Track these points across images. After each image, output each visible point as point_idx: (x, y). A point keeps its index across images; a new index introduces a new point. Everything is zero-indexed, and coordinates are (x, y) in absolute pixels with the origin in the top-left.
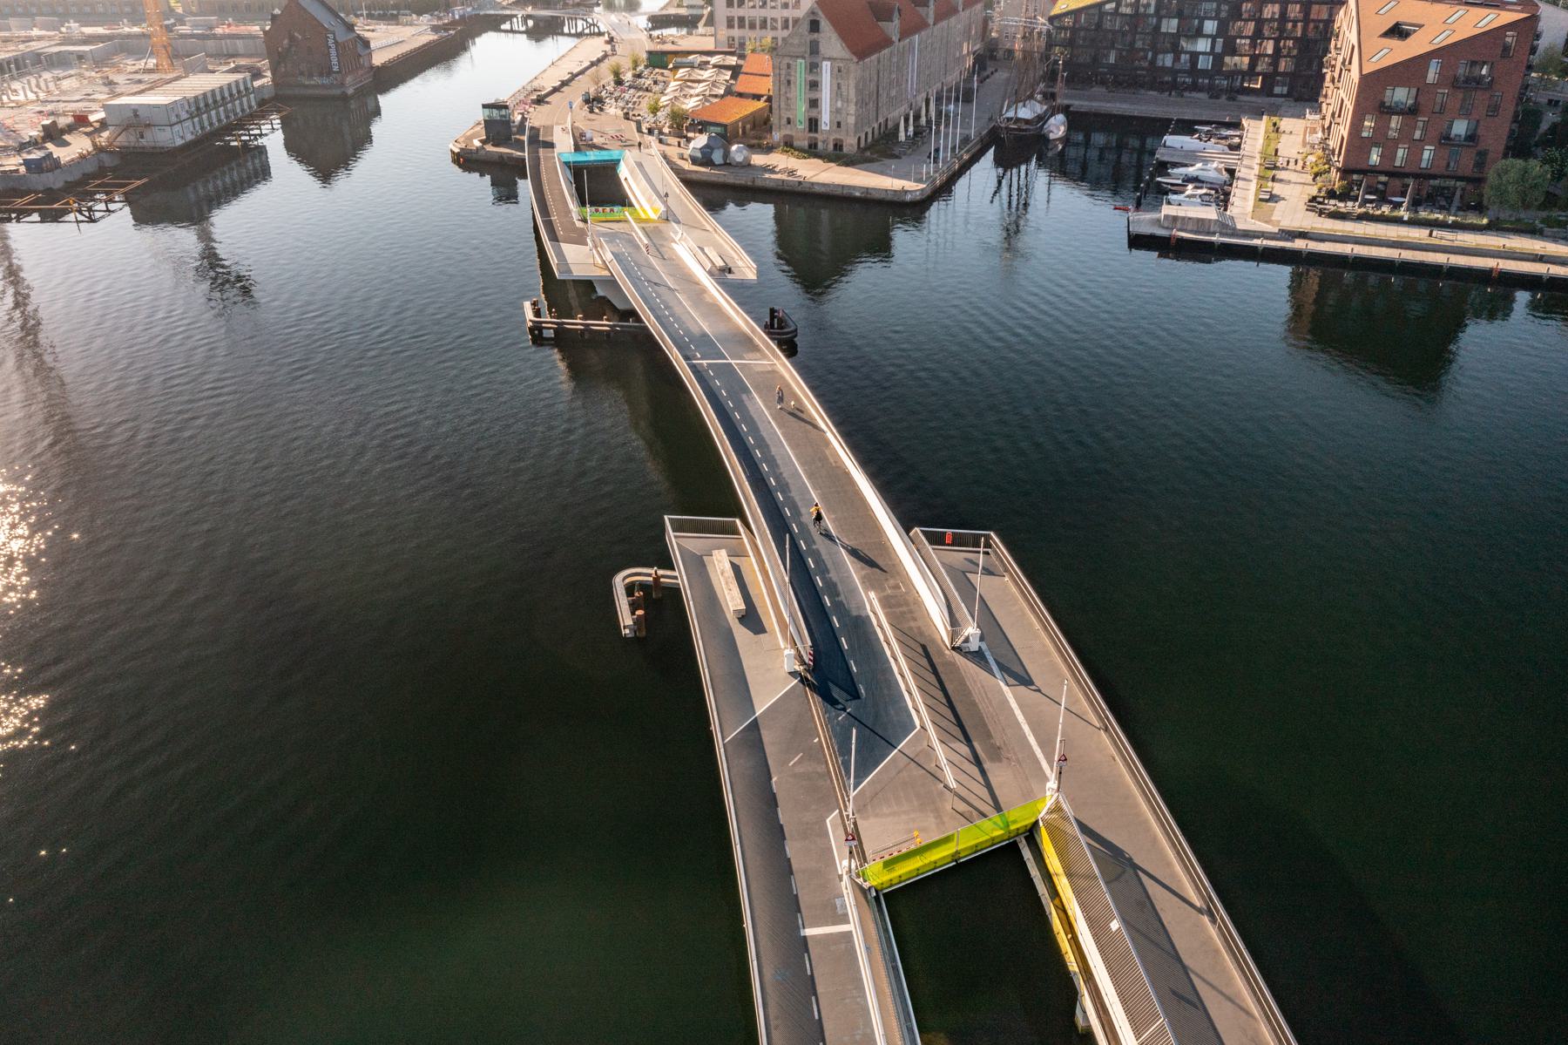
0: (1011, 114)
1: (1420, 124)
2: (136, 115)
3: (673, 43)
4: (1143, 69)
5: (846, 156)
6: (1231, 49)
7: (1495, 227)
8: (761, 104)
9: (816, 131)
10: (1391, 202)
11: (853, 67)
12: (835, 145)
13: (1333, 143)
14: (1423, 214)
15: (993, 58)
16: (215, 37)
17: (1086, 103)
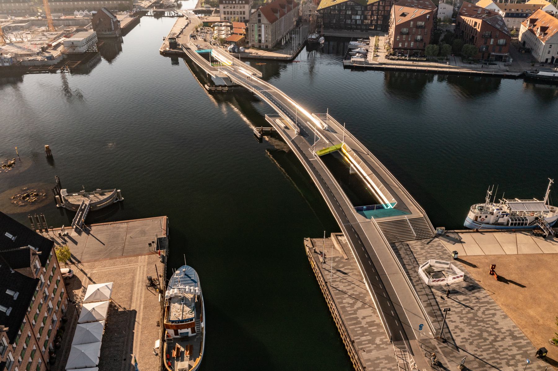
0: (310, 37)
1: (410, 37)
2: (73, 43)
3: (206, 19)
4: (343, 24)
5: (269, 49)
6: (365, 18)
7: (427, 61)
8: (243, 36)
9: (261, 43)
10: (404, 56)
11: (270, 26)
12: (266, 47)
13: (391, 42)
14: (412, 58)
15: (301, 21)
16: (62, 20)
17: (328, 34)
